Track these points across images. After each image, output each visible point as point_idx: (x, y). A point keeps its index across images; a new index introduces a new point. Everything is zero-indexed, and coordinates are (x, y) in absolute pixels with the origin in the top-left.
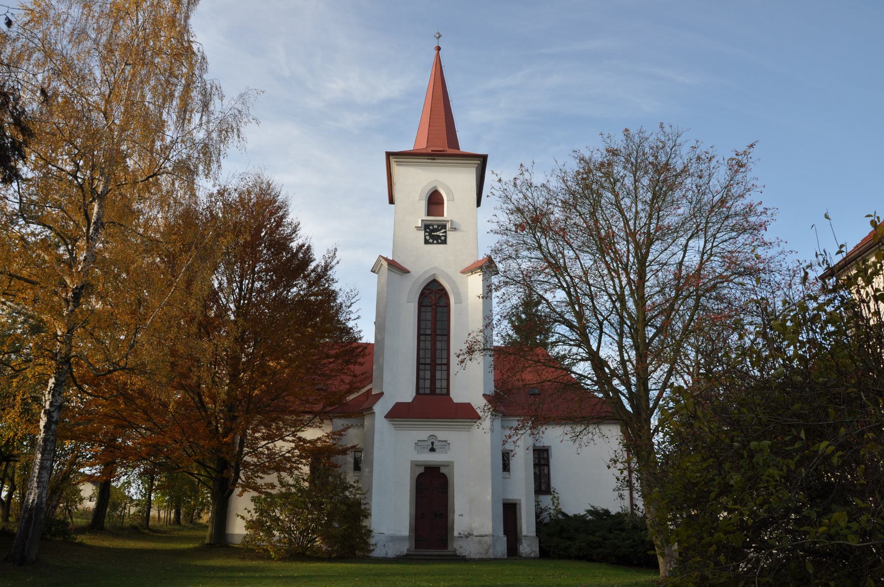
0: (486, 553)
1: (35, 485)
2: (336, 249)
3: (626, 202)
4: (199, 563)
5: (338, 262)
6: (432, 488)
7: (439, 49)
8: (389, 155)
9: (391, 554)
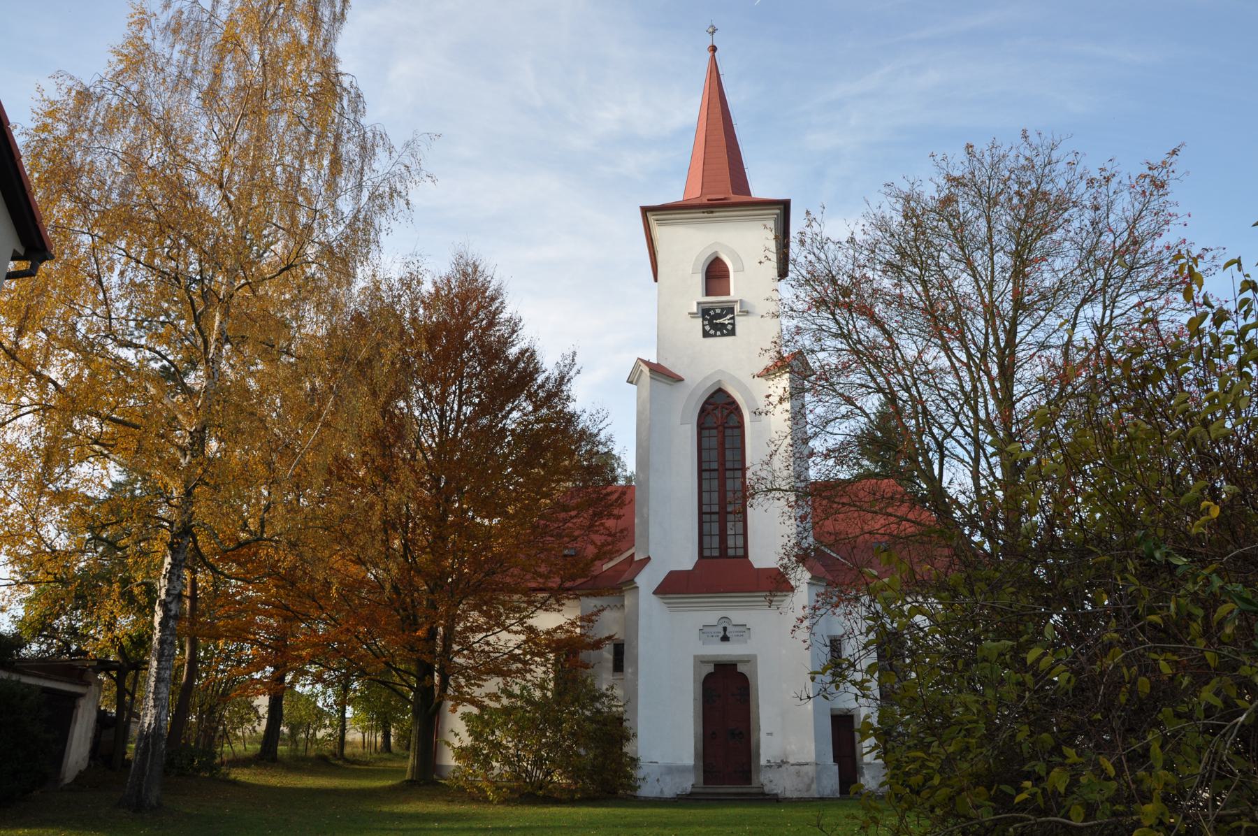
0: (808, 790)
1: (151, 703)
2: (575, 353)
3: (979, 258)
4: (386, 809)
5: (579, 372)
6: (726, 695)
7: (714, 49)
8: (645, 211)
9: (669, 792)
